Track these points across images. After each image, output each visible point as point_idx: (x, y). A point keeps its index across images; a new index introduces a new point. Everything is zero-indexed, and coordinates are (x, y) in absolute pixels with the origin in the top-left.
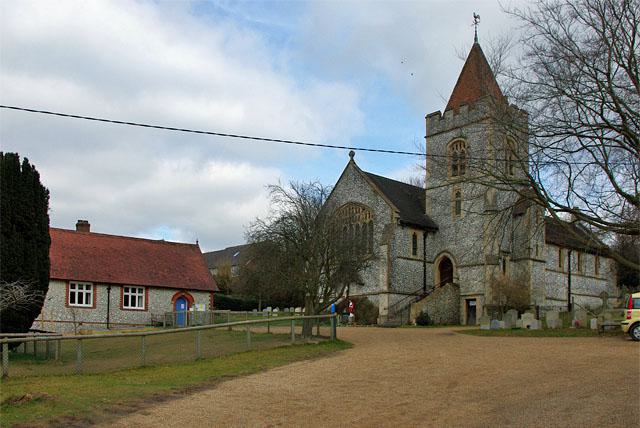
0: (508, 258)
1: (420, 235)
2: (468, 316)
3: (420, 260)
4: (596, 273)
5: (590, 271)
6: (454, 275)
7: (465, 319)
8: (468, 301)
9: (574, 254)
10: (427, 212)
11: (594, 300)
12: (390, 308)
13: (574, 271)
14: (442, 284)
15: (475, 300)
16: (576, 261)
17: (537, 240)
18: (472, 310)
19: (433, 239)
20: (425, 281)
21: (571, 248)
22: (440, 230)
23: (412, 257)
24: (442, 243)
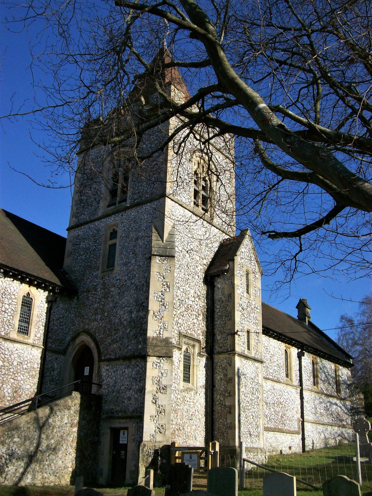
23: (14, 335)
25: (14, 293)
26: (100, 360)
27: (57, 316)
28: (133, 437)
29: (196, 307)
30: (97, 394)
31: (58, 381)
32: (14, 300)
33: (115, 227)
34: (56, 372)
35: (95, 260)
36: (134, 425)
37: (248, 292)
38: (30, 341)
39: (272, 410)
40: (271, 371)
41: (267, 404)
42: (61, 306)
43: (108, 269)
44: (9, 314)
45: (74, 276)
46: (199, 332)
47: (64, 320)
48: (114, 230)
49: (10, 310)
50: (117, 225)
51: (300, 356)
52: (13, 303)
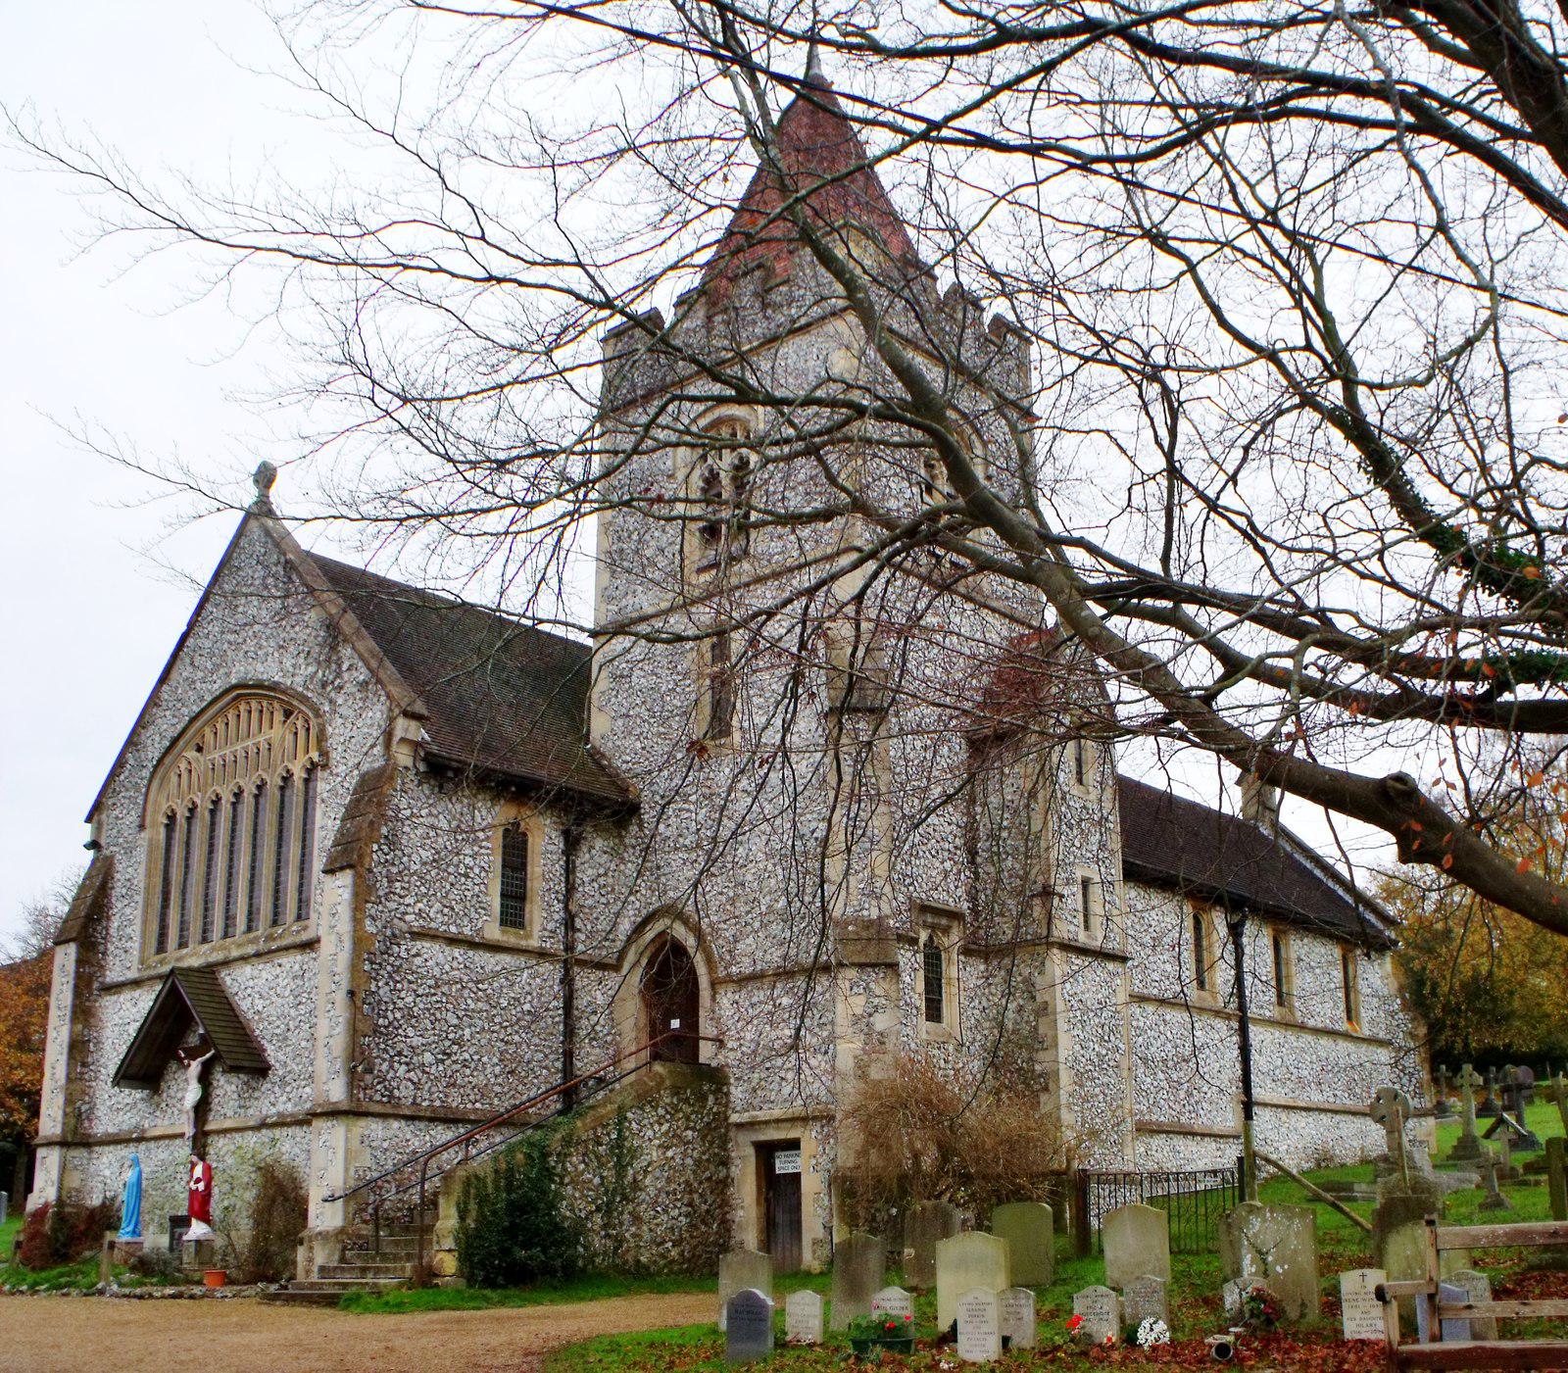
0: (955, 938)
1: (544, 839)
3: (542, 955)
4: (1350, 1013)
5: (1327, 1011)
6: (706, 1028)
8: (766, 1152)
9: (1258, 941)
10: (600, 725)
11: (1350, 1126)
12: (358, 1195)
13: (1261, 1000)
15: (794, 1145)
16: (1267, 970)
17: (1086, 860)
18: (780, 1195)
19: (614, 853)
20: (568, 1056)
21: (1240, 908)
22: (648, 815)
23: (494, 932)
26: (714, 985)
27: (590, 872)
29: (948, 829)
30: (714, 1064)
37: (1080, 781)
38: (534, 943)
39: (1161, 1076)
40: (1156, 976)
41: (1145, 1060)
42: (599, 843)
46: (959, 892)
51: (1235, 931)
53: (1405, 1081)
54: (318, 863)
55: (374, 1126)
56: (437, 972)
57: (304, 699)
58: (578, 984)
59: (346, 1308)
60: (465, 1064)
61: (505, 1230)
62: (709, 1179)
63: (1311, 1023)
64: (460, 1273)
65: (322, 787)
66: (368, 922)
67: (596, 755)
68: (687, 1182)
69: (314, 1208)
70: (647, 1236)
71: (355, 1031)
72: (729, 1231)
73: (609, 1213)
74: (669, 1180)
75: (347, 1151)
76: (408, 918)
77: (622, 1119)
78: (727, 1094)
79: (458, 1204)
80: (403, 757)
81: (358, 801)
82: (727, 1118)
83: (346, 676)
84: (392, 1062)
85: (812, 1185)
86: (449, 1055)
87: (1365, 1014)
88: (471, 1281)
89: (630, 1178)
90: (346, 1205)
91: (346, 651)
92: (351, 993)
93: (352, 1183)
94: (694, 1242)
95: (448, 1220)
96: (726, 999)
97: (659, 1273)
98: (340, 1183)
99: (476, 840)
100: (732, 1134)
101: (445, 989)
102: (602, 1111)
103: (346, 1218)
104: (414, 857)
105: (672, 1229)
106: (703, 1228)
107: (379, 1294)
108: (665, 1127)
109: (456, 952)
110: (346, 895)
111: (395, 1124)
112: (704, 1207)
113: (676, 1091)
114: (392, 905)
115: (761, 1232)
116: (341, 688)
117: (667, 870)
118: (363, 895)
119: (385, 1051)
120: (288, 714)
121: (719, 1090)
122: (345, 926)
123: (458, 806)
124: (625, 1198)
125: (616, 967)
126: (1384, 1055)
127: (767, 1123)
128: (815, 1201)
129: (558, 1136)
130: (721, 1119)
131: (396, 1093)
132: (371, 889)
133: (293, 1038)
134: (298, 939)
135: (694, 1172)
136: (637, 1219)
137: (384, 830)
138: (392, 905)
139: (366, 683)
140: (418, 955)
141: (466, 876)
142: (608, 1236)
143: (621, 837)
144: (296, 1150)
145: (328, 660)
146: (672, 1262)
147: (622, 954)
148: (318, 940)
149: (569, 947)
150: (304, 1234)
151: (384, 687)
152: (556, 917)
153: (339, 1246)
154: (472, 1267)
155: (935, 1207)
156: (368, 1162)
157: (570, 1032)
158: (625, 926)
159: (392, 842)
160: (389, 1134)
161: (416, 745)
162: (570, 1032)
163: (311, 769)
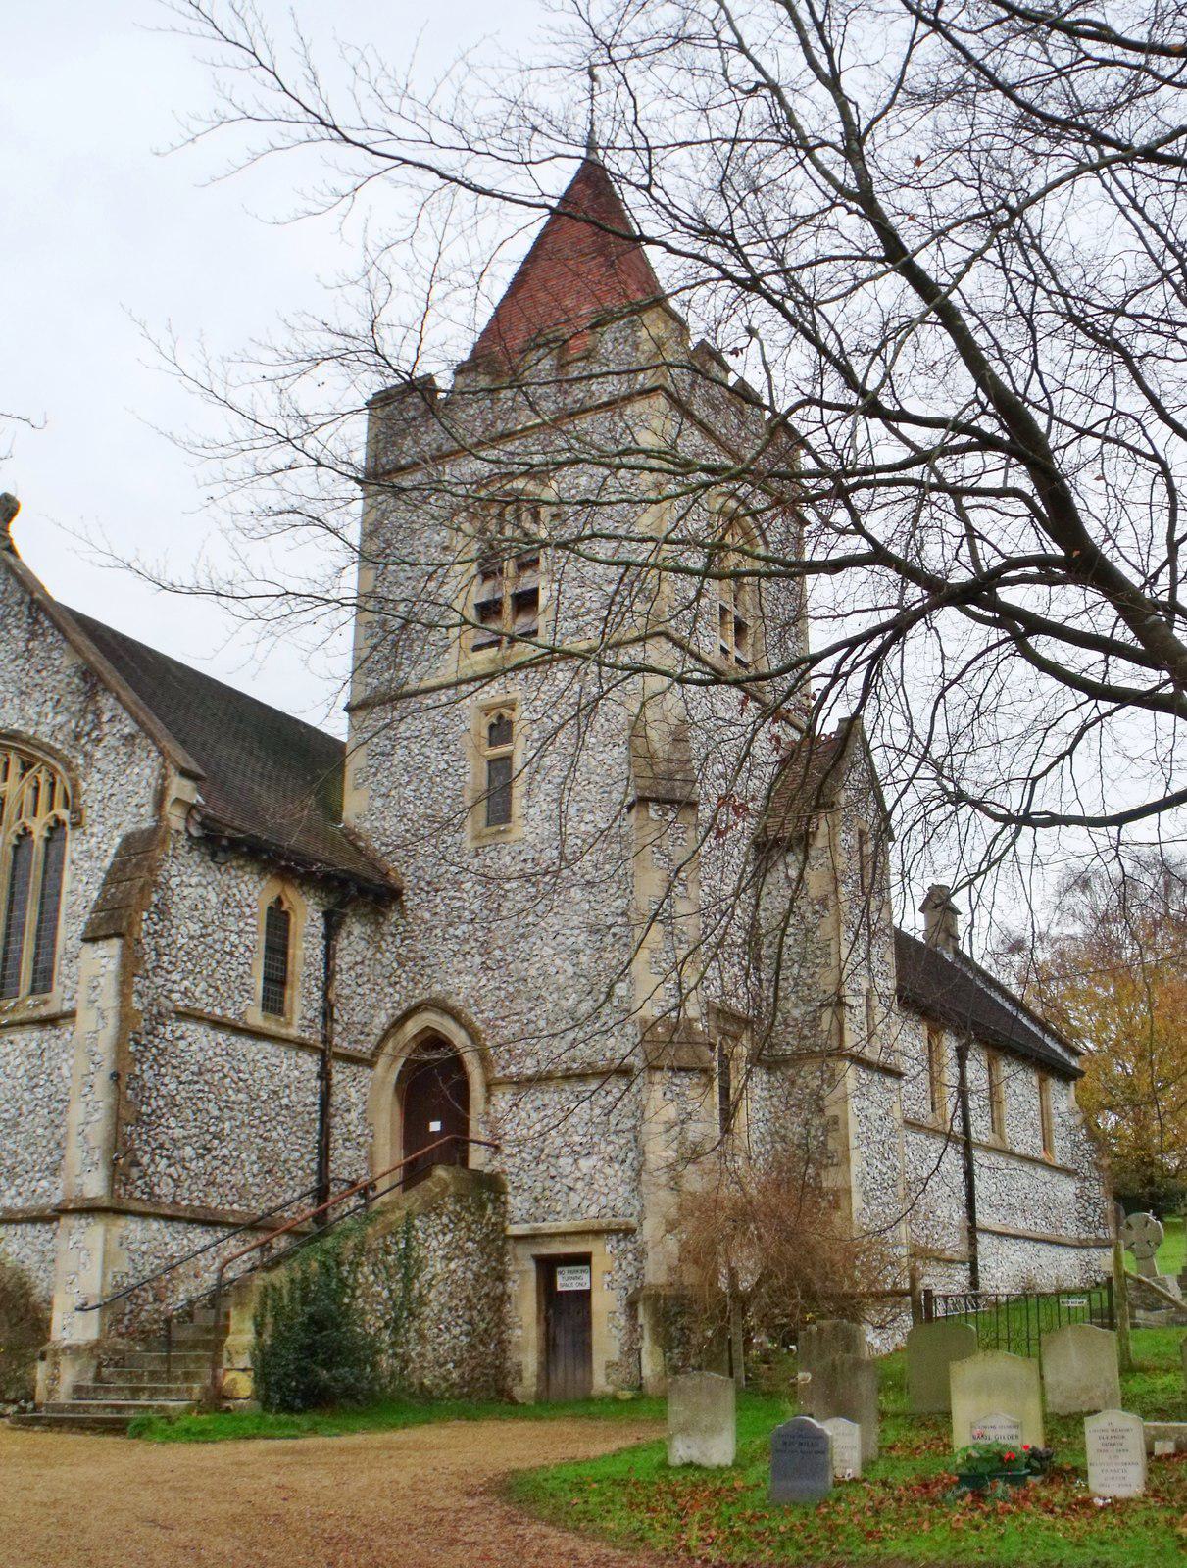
1: (307, 916)
2: (549, 1348)
3: (301, 1045)
4: (1047, 1145)
5: (1025, 1140)
6: (477, 1129)
7: (529, 1360)
8: (547, 1267)
12: (117, 1305)
14: (413, 1174)
15: (584, 1260)
18: (566, 1314)
19: (374, 942)
22: (411, 901)
23: (256, 1018)
24: (416, 963)
25: (250, 901)
26: (490, 1086)
27: (348, 959)
28: (608, 1278)
30: (487, 1170)
31: (361, 1139)
32: (250, 921)
33: (506, 712)
34: (353, 1116)
35: (449, 801)
36: (608, 1248)
38: (294, 1032)
42: (357, 929)
43: (494, 829)
44: (242, 961)
45: (383, 844)
47: (367, 970)
48: (500, 717)
49: (242, 949)
50: (511, 706)
52: (248, 928)
53: (1090, 1211)
54: (69, 932)
55: (133, 1226)
56: (200, 1057)
57: (51, 751)
58: (336, 1077)
59: (139, 1435)
60: (225, 1161)
61: (302, 1348)
62: (487, 1295)
63: (1018, 1150)
64: (255, 1396)
65: (73, 847)
66: (135, 998)
67: (351, 837)
68: (467, 1298)
69: (58, 1319)
70: (430, 1356)
71: (118, 1118)
72: (504, 1351)
73: (396, 1330)
74: (451, 1295)
75: (105, 1253)
76: (174, 996)
77: (410, 1227)
78: (505, 1203)
79: (255, 1317)
80: (175, 819)
81: (124, 864)
82: (504, 1230)
83: (106, 728)
84: (153, 1155)
85: (606, 1305)
86: (209, 1150)
87: (1057, 1143)
88: (266, 1403)
89: (415, 1292)
90: (102, 1317)
91: (106, 702)
92: (116, 1077)
93: (109, 1290)
94: (473, 1363)
95: (242, 1335)
96: (503, 1100)
97: (442, 1398)
98: (97, 1290)
99: (242, 916)
100: (509, 1246)
101: (207, 1077)
102: (392, 1217)
103: (101, 1330)
104: (183, 929)
105: (453, 1348)
106: (482, 1349)
107: (169, 1421)
108: (448, 1237)
109: (220, 1037)
110: (112, 966)
111: (155, 1225)
112: (483, 1326)
113: (459, 1198)
114: (159, 981)
115: (541, 1353)
116: (99, 740)
117: (433, 961)
118: (130, 968)
119: (147, 1142)
120: (26, 767)
121: (497, 1199)
122: (109, 1000)
123: (226, 878)
124: (411, 1314)
125: (370, 1064)
126: (1068, 1188)
127: (552, 1235)
128: (609, 1320)
129: (351, 1243)
130: (498, 1229)
131: (157, 1190)
132: (139, 961)
133: (25, 1124)
134: (36, 1014)
135: (474, 1287)
136: (422, 1337)
137: (154, 898)
138: (159, 981)
139: (132, 737)
140: (182, 1037)
141: (231, 954)
142: (395, 1355)
143: (379, 925)
144: (26, 1251)
145: (83, 711)
146: (452, 1385)
147: (375, 1055)
148: (71, 1015)
149: (327, 1040)
150: (48, 1346)
151: (155, 742)
152: (316, 1005)
153: (94, 1363)
154: (267, 1389)
155: (835, 1327)
156: (127, 1267)
157: (325, 1132)
158: (382, 1020)
159: (162, 911)
160: (148, 1235)
161: (191, 808)
162: (325, 1132)
163: (56, 827)
